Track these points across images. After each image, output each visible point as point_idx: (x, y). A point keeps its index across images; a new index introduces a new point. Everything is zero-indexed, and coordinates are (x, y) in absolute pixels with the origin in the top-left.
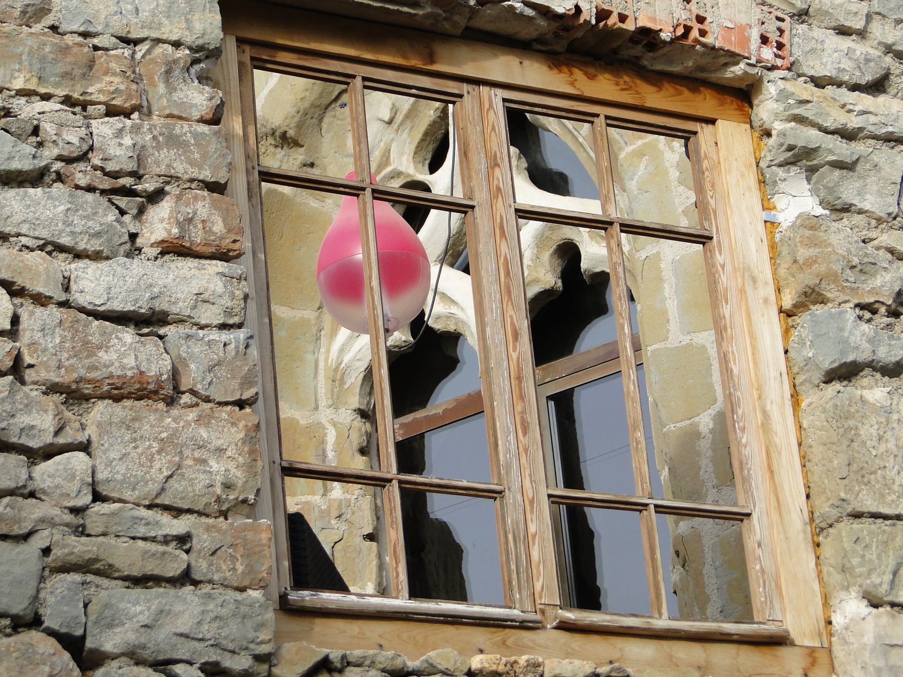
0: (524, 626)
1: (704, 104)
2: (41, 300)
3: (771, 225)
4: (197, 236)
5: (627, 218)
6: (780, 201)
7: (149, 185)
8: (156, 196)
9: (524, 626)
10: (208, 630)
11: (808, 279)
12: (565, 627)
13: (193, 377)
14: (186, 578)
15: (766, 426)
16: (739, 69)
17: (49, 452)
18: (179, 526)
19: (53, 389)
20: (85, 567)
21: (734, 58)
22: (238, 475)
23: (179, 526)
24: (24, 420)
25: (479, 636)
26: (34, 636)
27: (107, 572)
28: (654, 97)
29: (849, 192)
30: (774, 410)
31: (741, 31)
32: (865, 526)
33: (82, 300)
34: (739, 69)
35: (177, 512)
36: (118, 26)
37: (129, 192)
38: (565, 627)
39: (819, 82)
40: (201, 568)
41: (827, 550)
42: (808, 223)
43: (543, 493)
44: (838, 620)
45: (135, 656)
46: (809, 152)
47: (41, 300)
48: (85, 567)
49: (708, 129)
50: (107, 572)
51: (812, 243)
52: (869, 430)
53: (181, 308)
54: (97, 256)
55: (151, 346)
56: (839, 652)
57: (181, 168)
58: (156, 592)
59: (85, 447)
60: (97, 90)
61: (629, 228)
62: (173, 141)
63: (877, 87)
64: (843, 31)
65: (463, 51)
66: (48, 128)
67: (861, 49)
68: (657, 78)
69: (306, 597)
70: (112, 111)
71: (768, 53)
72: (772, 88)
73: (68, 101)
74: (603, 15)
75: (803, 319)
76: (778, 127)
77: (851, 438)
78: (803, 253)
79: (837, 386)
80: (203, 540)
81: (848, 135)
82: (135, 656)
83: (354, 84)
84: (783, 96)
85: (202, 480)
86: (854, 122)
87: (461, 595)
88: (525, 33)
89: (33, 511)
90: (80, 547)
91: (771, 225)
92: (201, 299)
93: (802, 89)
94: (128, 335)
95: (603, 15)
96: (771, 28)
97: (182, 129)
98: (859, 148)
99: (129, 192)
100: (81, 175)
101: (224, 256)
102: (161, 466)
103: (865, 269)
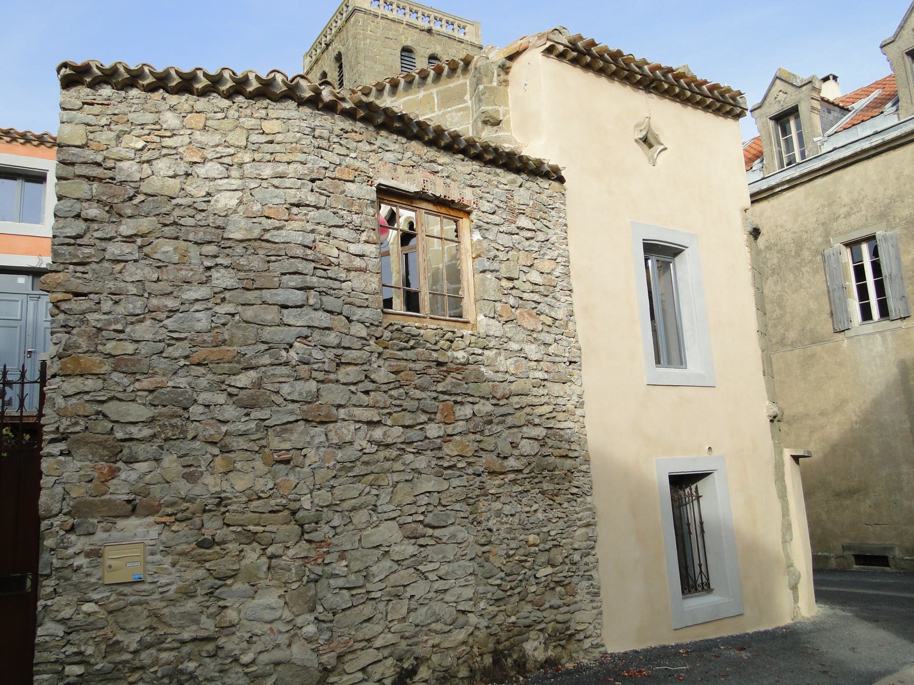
0: (424, 317)
1: (461, 215)
2: (343, 251)
3: (472, 240)
4: (371, 240)
5: (446, 237)
6: (473, 235)
7: (363, 229)
8: (363, 231)
9: (424, 317)
10: (371, 317)
11: (478, 252)
12: (431, 318)
13: (370, 267)
14: (367, 307)
15: (468, 281)
16: (469, 209)
17: (344, 281)
18: (366, 296)
19: (345, 269)
20: (350, 304)
21: (468, 206)
22: (377, 287)
23: (366, 296)
24: (340, 275)
25: (416, 319)
26: (341, 316)
27: (354, 305)
28: (452, 213)
29: (487, 235)
30: (470, 277)
31: (470, 201)
32: (485, 301)
33: (351, 252)
34: (469, 209)
35: (366, 294)
36: (358, 196)
37: (358, 230)
38: (431, 318)
39: (483, 212)
40: (370, 305)
41: (477, 305)
42: (479, 241)
43: (428, 292)
44: (478, 319)
45: (358, 321)
46: (480, 227)
47: (343, 251)
48: (350, 304)
49: (461, 220)
50: (354, 305)
51: (479, 245)
52: (487, 283)
53: (368, 254)
54: (353, 243)
55: (362, 261)
56: (478, 325)
57: (368, 226)
58: (56, 337)
59: (350, 281)
60: (354, 209)
61: (445, 239)
62: (367, 220)
63: (493, 213)
64: (488, 201)
65: (417, 202)
66: (345, 217)
67: (492, 205)
68: (453, 209)
69: (385, 310)
70: (356, 213)
71: (474, 206)
72: (474, 213)
73: (348, 211)
74: (445, 196)
75: (476, 260)
76: (475, 221)
77: (484, 284)
78: (478, 247)
79: (482, 274)
80: (370, 300)
81: (488, 223)
82: (358, 321)
83: (132, 119)
84: (476, 215)
85: (371, 288)
86: (489, 221)
87: (418, 312)
88: (430, 199)
89: (342, 293)
90: (349, 300)
91: (472, 240)
92: (371, 252)
93: (480, 213)
94: (358, 259)
95: (445, 196)
96: (475, 200)
97: (369, 217)
98: (490, 226)
99: (358, 230)
100: (351, 226)
101: (375, 244)
102: (364, 285)
103: (489, 251)
